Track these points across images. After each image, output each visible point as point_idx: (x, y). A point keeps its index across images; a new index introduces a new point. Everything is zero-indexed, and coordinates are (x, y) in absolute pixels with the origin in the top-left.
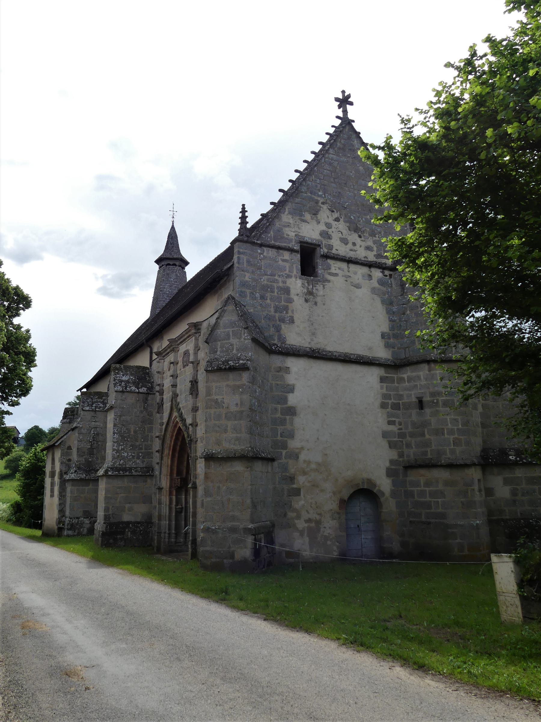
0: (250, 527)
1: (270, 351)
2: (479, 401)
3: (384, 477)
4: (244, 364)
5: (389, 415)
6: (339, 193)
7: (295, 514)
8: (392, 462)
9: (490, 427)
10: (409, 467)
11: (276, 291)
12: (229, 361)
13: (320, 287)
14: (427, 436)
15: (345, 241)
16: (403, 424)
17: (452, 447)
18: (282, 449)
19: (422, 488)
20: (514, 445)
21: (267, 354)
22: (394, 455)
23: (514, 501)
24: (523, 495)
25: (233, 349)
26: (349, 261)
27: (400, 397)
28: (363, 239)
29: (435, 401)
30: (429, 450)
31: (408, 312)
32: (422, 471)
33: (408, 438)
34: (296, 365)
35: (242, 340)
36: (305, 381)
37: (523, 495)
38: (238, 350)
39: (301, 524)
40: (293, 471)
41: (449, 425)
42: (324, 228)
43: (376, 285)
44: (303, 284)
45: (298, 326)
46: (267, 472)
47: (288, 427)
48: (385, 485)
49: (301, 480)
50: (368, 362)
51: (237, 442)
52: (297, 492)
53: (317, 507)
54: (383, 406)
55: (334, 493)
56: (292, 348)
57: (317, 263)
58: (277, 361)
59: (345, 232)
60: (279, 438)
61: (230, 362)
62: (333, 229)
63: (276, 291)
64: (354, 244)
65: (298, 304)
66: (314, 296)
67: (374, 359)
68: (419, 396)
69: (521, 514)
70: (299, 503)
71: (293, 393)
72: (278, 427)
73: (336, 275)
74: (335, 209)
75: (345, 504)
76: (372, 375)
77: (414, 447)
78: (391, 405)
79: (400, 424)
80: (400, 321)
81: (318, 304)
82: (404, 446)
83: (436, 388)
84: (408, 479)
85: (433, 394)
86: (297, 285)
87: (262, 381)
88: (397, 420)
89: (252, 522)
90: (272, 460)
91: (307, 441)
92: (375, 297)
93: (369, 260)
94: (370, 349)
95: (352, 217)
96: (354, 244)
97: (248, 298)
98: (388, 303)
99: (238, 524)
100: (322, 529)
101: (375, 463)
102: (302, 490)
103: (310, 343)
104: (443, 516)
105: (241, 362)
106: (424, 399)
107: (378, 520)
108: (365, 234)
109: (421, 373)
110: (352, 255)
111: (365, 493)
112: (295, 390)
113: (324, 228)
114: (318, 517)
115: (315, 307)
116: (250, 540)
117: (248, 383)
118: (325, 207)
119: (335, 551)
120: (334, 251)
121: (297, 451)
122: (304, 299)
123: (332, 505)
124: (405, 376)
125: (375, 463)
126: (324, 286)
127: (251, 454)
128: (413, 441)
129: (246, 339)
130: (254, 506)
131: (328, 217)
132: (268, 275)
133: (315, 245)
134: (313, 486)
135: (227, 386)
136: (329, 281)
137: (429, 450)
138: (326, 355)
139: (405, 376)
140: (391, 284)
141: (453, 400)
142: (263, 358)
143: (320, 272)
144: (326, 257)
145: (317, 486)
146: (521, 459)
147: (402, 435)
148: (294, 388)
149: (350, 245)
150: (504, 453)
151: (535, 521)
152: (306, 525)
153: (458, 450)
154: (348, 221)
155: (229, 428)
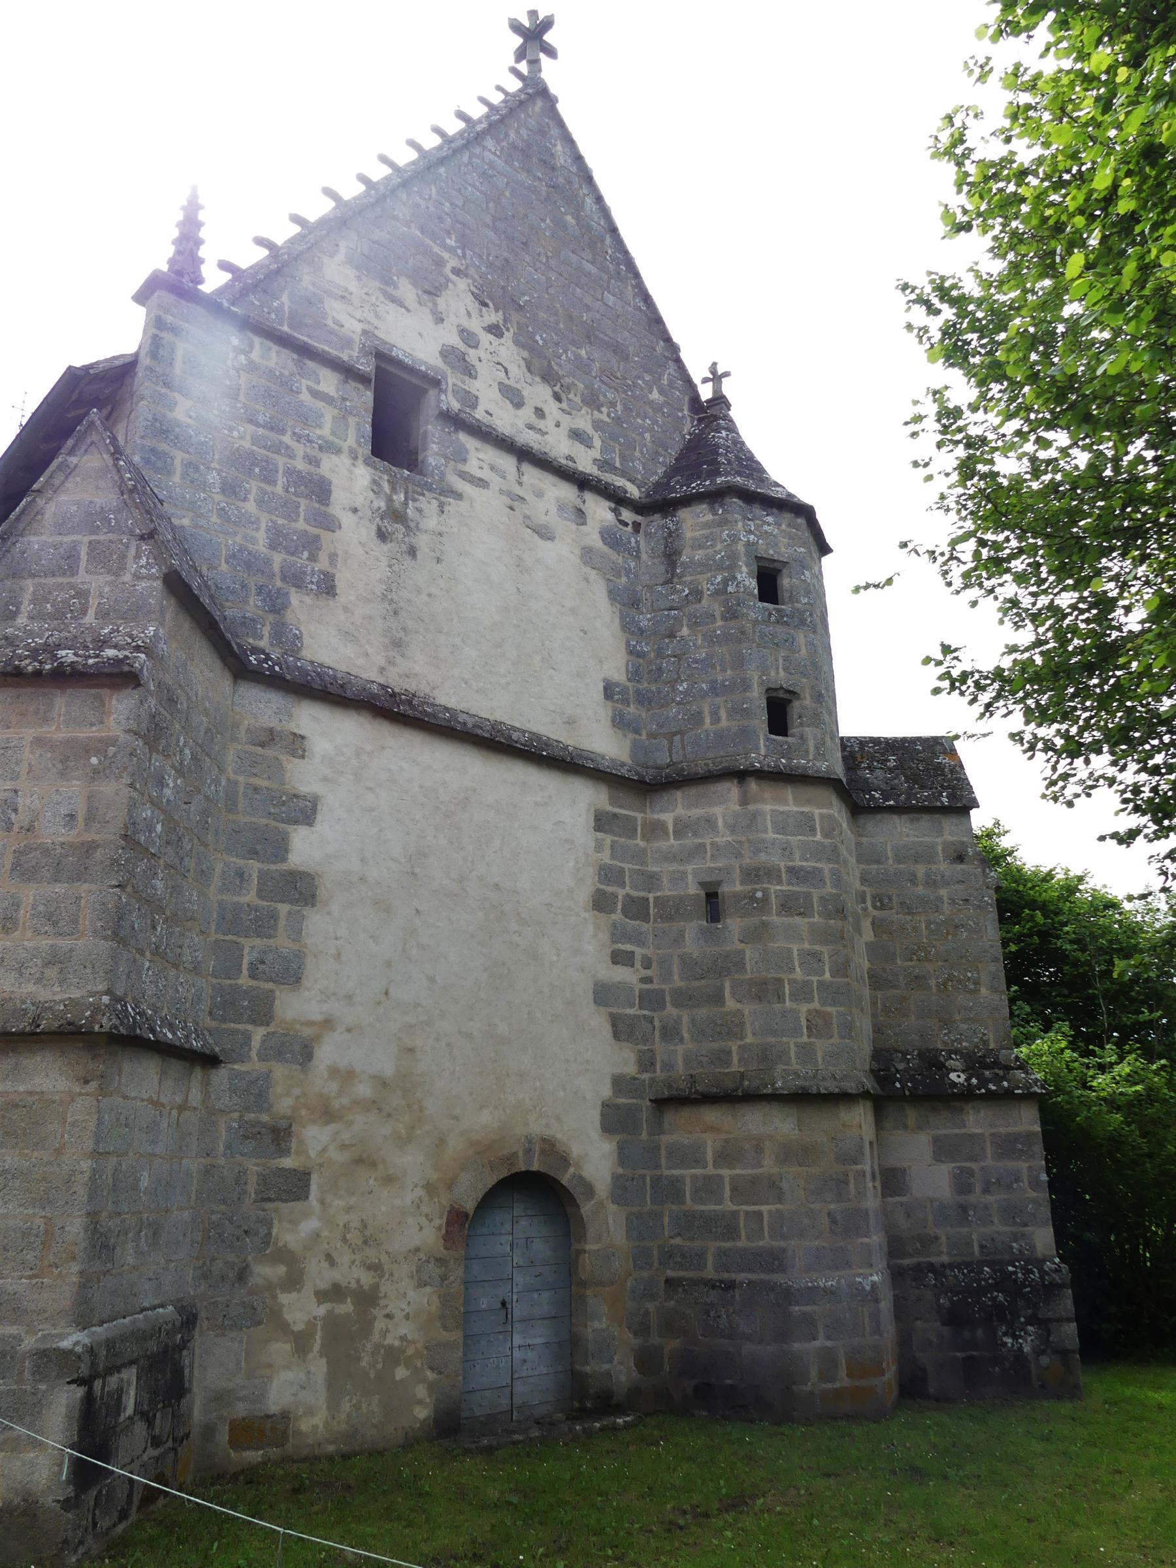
0: (66, 1344)
1: (240, 667)
2: (865, 909)
3: (595, 1132)
4: (118, 662)
5: (619, 934)
6: (506, 260)
7: (282, 1270)
8: (618, 1082)
9: (895, 987)
10: (671, 1101)
11: (281, 480)
12: (59, 647)
13: (428, 503)
14: (731, 1004)
15: (515, 398)
16: (654, 964)
17: (805, 1039)
18: (253, 1022)
19: (710, 1170)
20: (960, 1041)
21: (227, 674)
22: (625, 1060)
23: (964, 1208)
24: (986, 1191)
25: (84, 612)
26: (525, 455)
27: (652, 880)
28: (564, 405)
29: (759, 895)
30: (734, 1048)
31: (685, 631)
32: (711, 1115)
33: (671, 1010)
34: (328, 733)
35: (127, 578)
36: (357, 796)
37: (986, 1191)
38: (103, 614)
39: (301, 1309)
40: (284, 1105)
41: (798, 969)
42: (455, 340)
43: (595, 541)
44: (374, 482)
45: (346, 609)
46: (182, 1108)
47: (282, 942)
48: (595, 1159)
49: (315, 1139)
50: (563, 761)
51: (52, 972)
52: (296, 1186)
53: (365, 1242)
54: (601, 903)
55: (430, 1188)
56: (318, 674)
57: (426, 432)
58: (261, 707)
59: (517, 371)
60: (244, 981)
61: (63, 653)
62: (480, 352)
63: (281, 480)
64: (540, 413)
65: (354, 536)
66: (407, 527)
67: (580, 753)
68: (708, 879)
69: (982, 1247)
70: (299, 1227)
71: (310, 824)
72: (241, 940)
73: (482, 483)
74: (492, 299)
75: (462, 1225)
76: (577, 802)
77: (686, 1035)
78: (624, 902)
79: (647, 964)
80: (660, 654)
81: (419, 555)
82: (657, 1033)
83: (763, 857)
84: (666, 1139)
85: (753, 874)
86: (354, 481)
87: (194, 758)
88: (639, 951)
89: (83, 1322)
90: (210, 1061)
91: (349, 997)
92: (593, 574)
93: (580, 469)
94: (571, 722)
95: (538, 338)
96: (540, 413)
97: (177, 478)
98: (627, 601)
99: (13, 1330)
100: (379, 1325)
101: (564, 1088)
102: (314, 1178)
103: (382, 670)
104: (775, 1260)
105: (110, 653)
106: (725, 889)
107: (569, 1280)
108: (571, 396)
109: (718, 811)
110: (529, 438)
111: (534, 1187)
112: (319, 817)
113: (455, 340)
114: (367, 1279)
115: (408, 562)
116: (63, 1401)
117: (129, 737)
118: (462, 284)
119: (420, 1402)
120: (479, 414)
121: (307, 1032)
122: (374, 527)
123: (422, 1232)
124: (668, 818)
125: (564, 1088)
126: (441, 506)
127: (106, 1022)
128: (685, 1019)
129: (142, 576)
130: (101, 1245)
131: (469, 314)
132: (258, 425)
133: (424, 376)
134: (359, 1161)
135: (39, 742)
136: (459, 496)
137: (734, 1048)
138: (434, 716)
139: (668, 818)
140: (638, 551)
141: (808, 896)
142: (204, 674)
143: (432, 461)
144: (457, 422)
145: (374, 1165)
146: (983, 1082)
147: (651, 1000)
148: (314, 810)
149: (527, 414)
150: (933, 1062)
151: (1022, 1268)
152: (322, 1311)
153: (822, 1047)
154: (524, 342)
155: (23, 914)
